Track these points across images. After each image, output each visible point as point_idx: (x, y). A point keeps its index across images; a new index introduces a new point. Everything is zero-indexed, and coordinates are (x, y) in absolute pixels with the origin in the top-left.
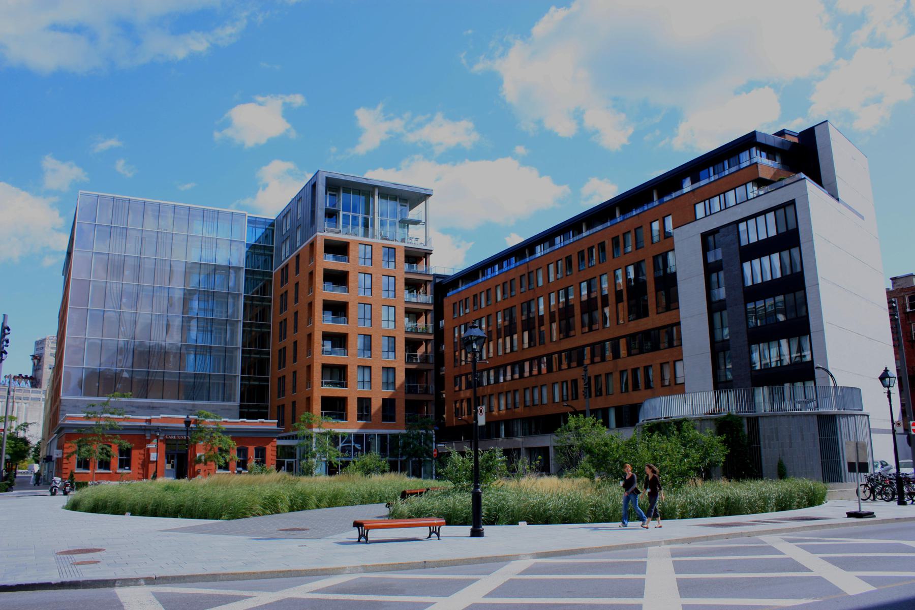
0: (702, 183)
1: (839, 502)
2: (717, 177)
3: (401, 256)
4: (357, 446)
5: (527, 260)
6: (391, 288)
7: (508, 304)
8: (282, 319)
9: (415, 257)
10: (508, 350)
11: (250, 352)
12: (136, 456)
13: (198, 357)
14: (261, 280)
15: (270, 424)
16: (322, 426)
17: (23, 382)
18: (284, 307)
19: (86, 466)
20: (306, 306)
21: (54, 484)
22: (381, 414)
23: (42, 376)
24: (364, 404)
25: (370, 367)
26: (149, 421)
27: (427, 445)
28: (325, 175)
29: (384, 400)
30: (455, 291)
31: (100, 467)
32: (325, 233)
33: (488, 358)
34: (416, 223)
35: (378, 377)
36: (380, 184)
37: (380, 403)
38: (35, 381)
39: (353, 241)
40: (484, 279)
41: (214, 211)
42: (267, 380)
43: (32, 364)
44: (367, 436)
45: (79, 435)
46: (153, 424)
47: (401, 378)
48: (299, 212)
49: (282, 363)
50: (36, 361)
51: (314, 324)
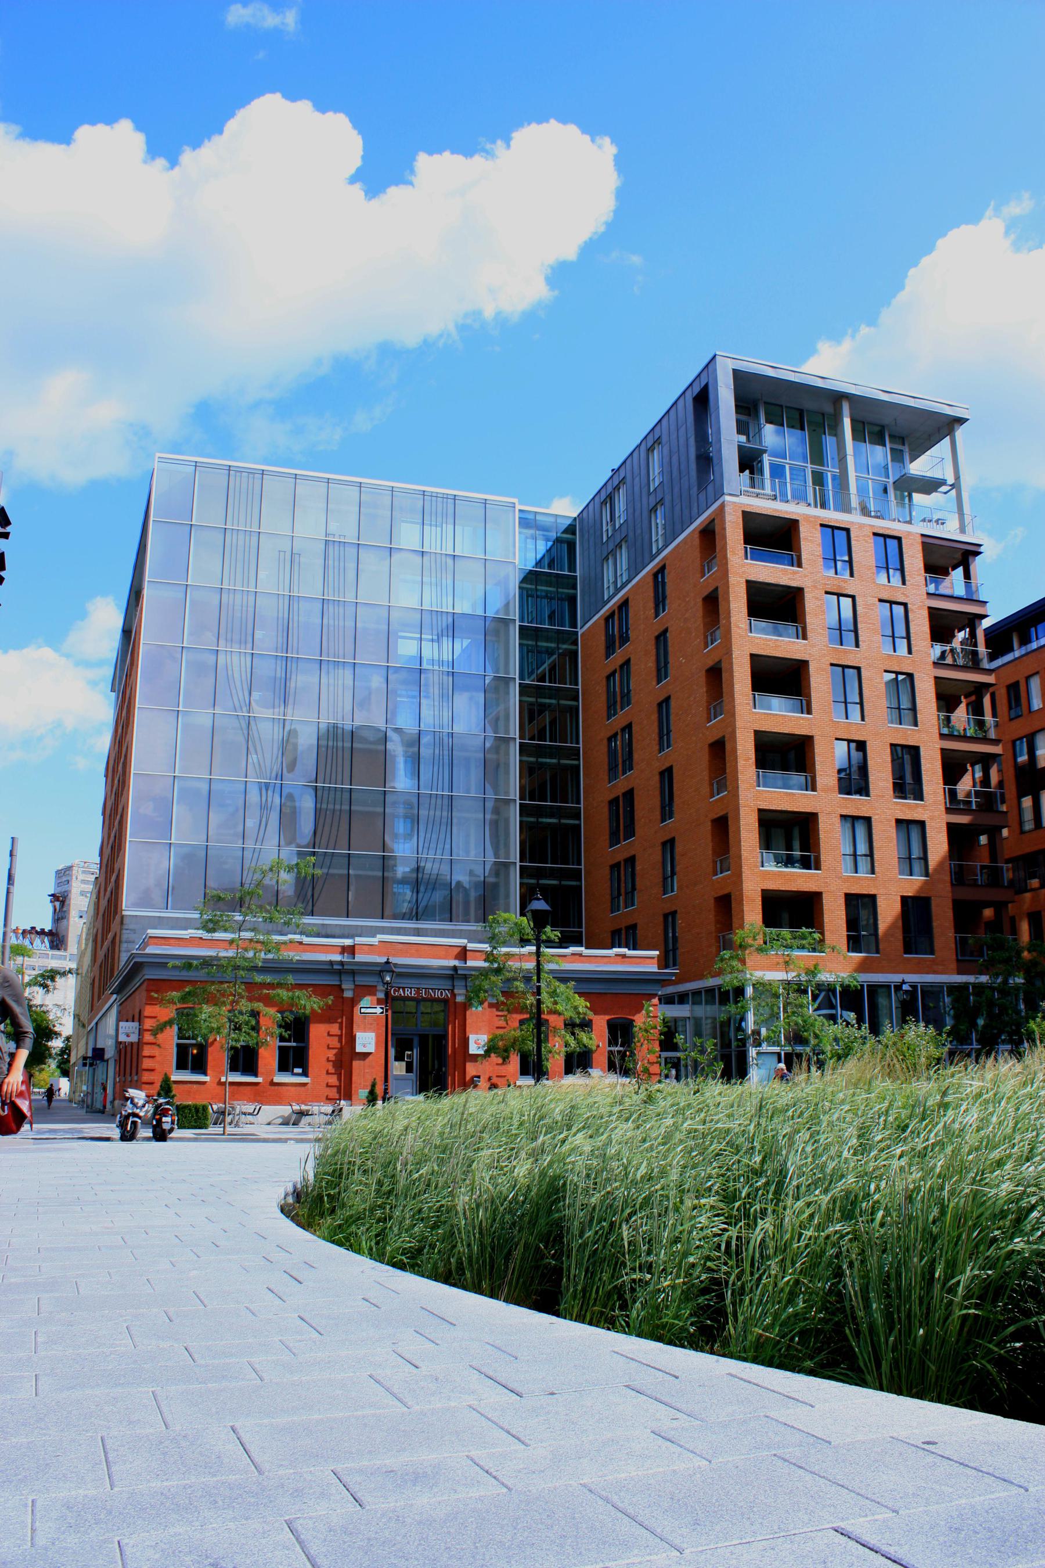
0: (1034, 645)
1: (26, 1127)
2: (1023, 651)
3: (914, 560)
6: (901, 630)
9: (948, 558)
10: (1029, 826)
11: (539, 812)
12: (321, 1038)
14: (550, 652)
15: (644, 960)
16: (768, 967)
17: (37, 941)
19: (199, 1065)
21: (129, 1108)
22: (899, 934)
23: (67, 929)
24: (860, 907)
25: (868, 820)
26: (351, 950)
28: (731, 365)
29: (904, 899)
31: (234, 1068)
32: (740, 498)
34: (930, 486)
35: (887, 843)
36: (852, 390)
37: (897, 907)
38: (56, 939)
39: (807, 517)
40: (1023, 651)
41: (445, 497)
42: (576, 875)
43: (51, 909)
44: (874, 989)
45: (191, 982)
46: (359, 958)
47: (938, 845)
50: (57, 904)
51: (733, 715)
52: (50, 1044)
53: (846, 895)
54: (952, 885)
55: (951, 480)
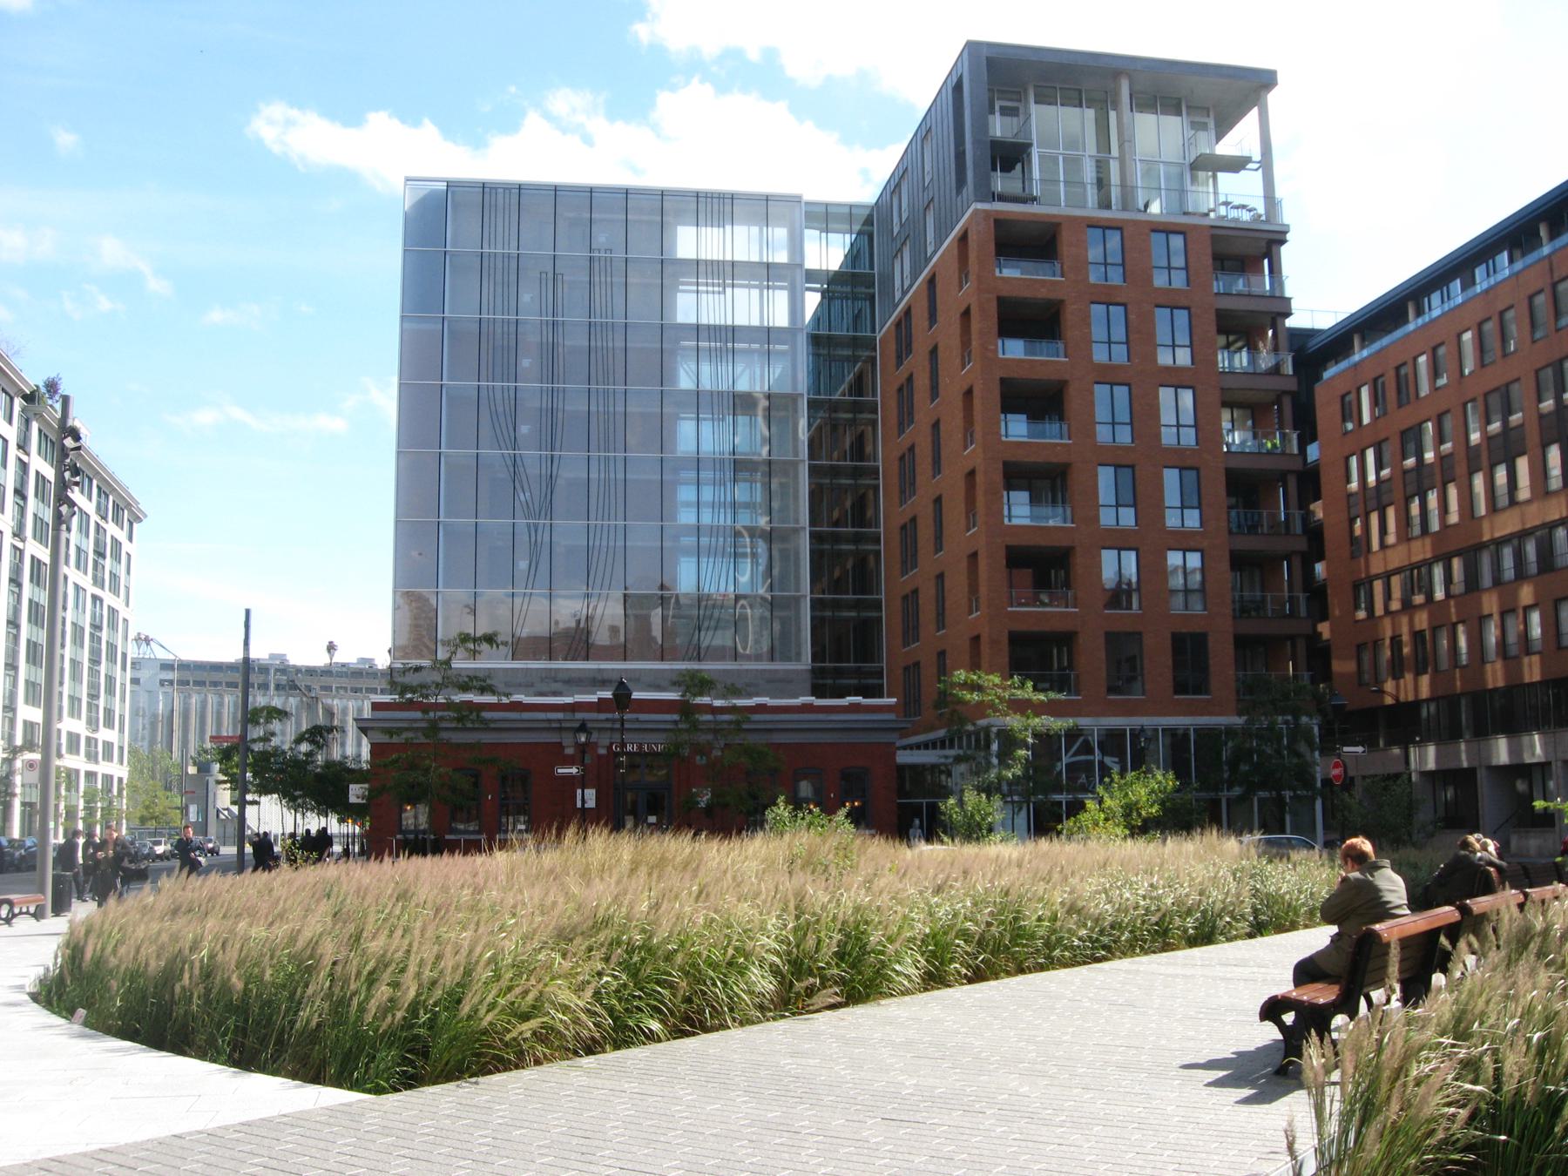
4: (1108, 760)
5: (1546, 250)
7: (1494, 378)
8: (906, 519)
13: (704, 560)
18: (907, 484)
20: (958, 402)
27: (1299, 755)
30: (1343, 365)
33: (1444, 526)
34: (1236, 164)
42: (877, 605)
44: (1136, 734)
48: (927, 168)
49: (909, 558)
52: (1334, 929)
53: (1107, 634)
54: (1234, 618)
55: (1257, 156)
